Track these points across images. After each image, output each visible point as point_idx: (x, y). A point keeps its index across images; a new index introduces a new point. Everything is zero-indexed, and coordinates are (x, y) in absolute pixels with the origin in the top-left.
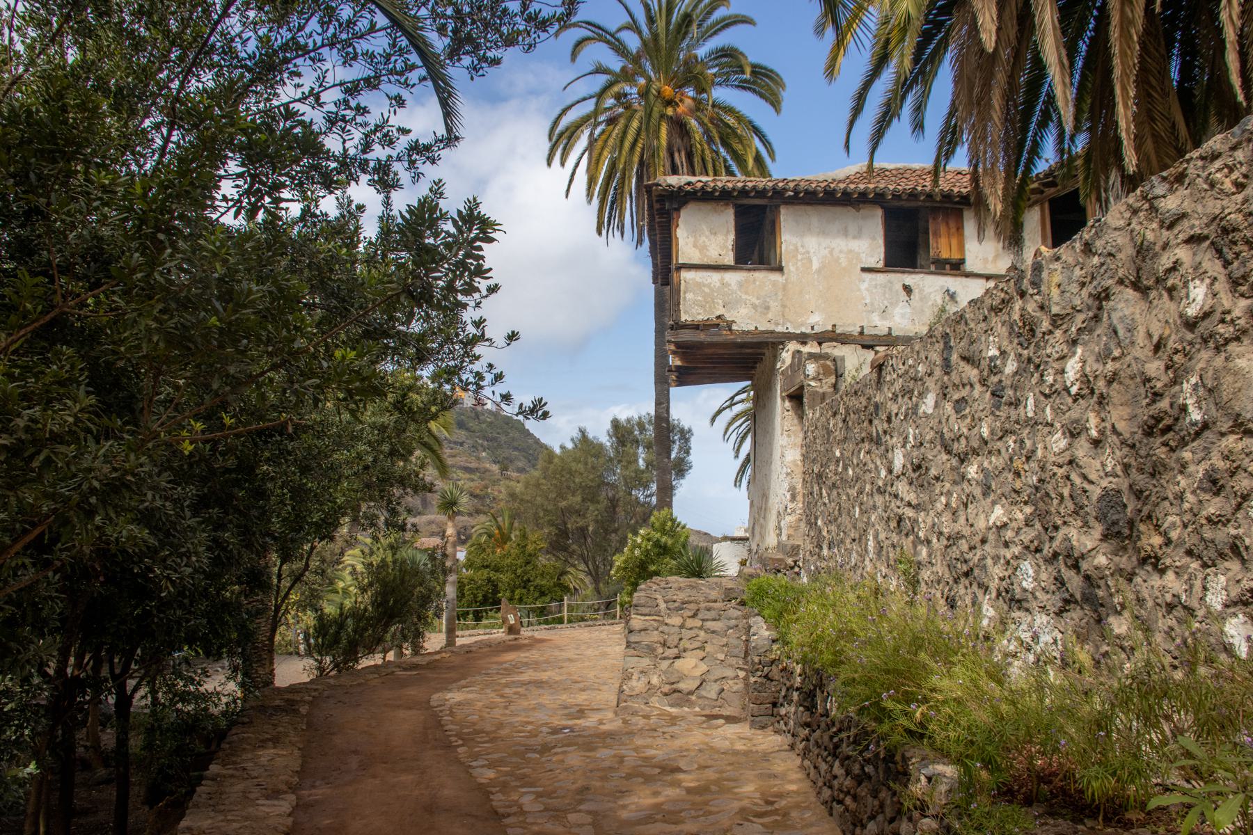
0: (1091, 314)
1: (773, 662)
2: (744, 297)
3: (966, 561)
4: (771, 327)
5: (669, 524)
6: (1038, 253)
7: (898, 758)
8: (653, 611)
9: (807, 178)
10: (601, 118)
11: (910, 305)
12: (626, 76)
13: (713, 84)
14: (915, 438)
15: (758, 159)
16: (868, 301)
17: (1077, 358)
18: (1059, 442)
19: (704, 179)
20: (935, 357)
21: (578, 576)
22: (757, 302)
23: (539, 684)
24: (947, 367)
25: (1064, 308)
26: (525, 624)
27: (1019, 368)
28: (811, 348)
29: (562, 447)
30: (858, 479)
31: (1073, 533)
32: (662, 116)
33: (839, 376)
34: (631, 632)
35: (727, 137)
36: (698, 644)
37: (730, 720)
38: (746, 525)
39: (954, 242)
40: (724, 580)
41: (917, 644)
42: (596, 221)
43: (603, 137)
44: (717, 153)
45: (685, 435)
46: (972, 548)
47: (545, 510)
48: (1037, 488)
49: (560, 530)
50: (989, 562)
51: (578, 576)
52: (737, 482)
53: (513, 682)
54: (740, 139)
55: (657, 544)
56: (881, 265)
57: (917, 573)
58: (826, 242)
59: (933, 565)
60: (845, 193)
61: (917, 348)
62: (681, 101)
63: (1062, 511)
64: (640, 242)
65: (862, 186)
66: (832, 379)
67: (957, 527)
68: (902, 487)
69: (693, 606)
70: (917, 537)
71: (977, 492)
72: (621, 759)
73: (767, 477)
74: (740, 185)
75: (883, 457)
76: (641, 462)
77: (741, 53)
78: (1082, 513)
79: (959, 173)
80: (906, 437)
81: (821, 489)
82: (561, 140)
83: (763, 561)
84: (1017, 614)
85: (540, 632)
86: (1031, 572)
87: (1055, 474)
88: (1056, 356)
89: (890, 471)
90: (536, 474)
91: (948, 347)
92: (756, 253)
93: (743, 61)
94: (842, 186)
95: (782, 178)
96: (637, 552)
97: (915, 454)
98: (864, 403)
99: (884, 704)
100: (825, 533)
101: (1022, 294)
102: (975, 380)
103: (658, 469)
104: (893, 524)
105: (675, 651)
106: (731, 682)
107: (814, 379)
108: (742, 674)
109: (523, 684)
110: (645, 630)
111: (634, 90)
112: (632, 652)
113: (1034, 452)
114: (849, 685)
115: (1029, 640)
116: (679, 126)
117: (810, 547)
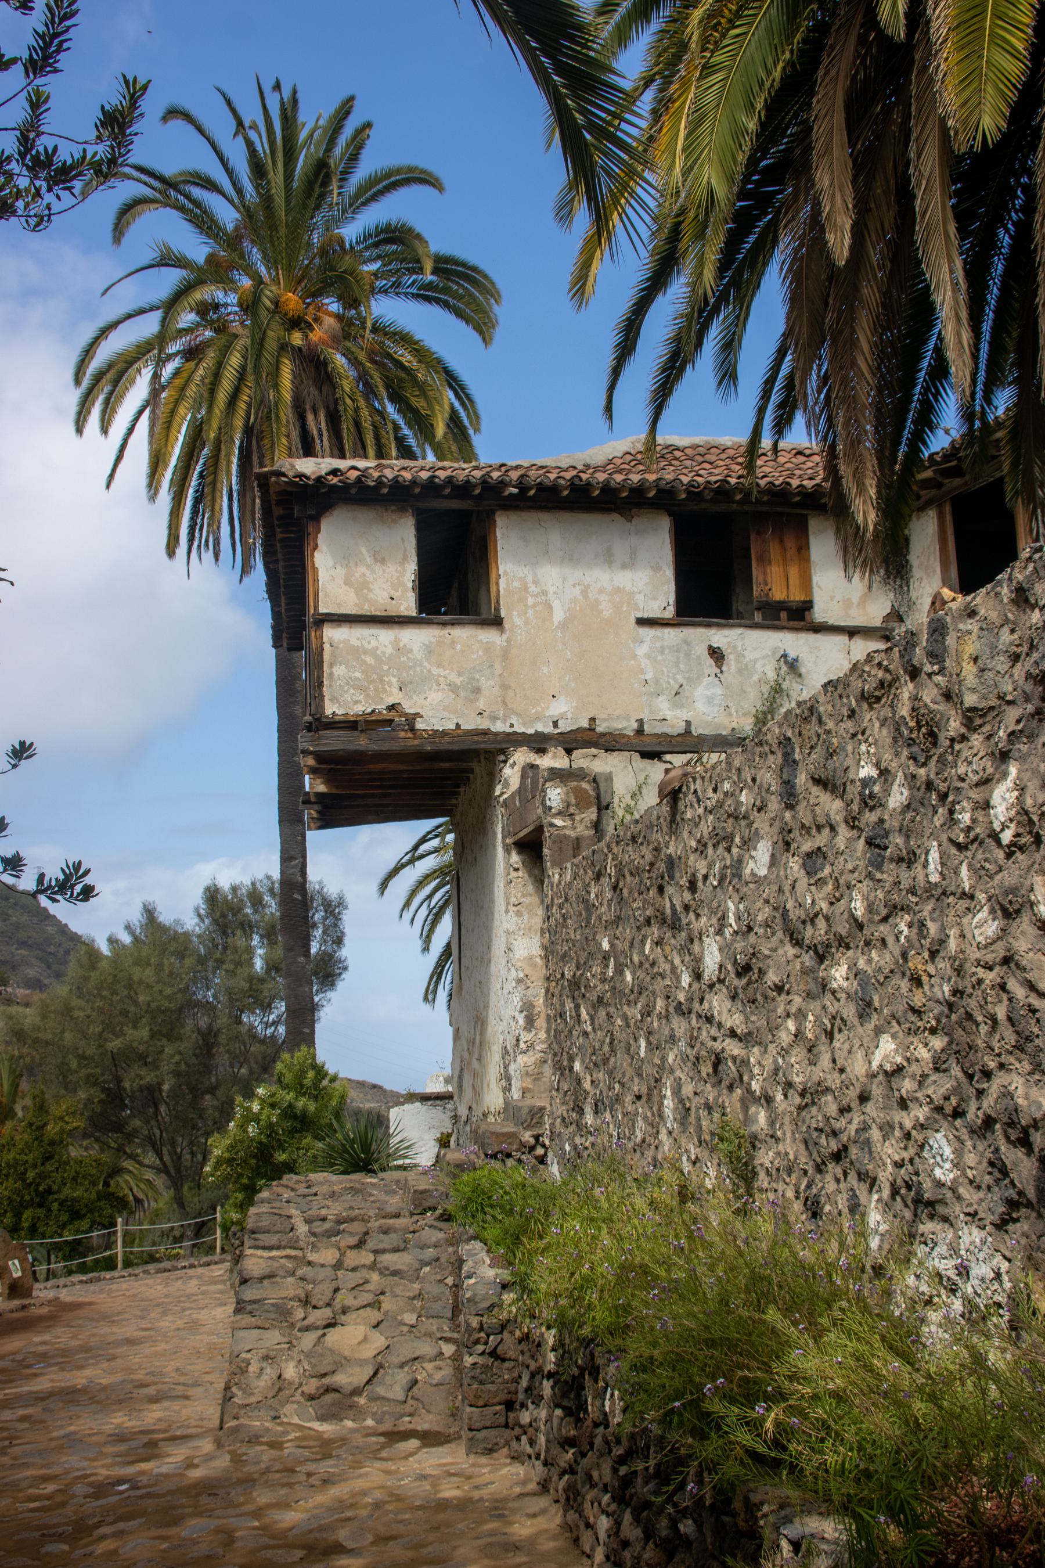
0: (1030, 708)
1: (503, 1327)
2: (435, 671)
3: (835, 1134)
4: (483, 724)
5: (311, 1074)
6: (938, 602)
7: (737, 1505)
8: (285, 1239)
9: (540, 462)
10: (173, 348)
11: (719, 681)
12: (215, 271)
13: (373, 291)
14: (739, 918)
15: (454, 419)
16: (649, 676)
17: (1009, 783)
18: (984, 925)
19: (361, 464)
20: (769, 778)
21: (143, 1177)
22: (458, 680)
23: (70, 1396)
24: (790, 797)
25: (985, 697)
26: (41, 1276)
27: (911, 798)
28: (553, 760)
29: (112, 941)
30: (641, 990)
31: (1017, 1084)
32: (284, 347)
33: (603, 807)
34: (244, 1281)
35: (401, 386)
36: (366, 1298)
37: (430, 1439)
38: (448, 1071)
39: (794, 572)
40: (411, 1175)
41: (760, 1289)
42: (165, 533)
43: (178, 382)
44: (382, 414)
45: (334, 909)
46: (844, 1110)
47: (83, 1057)
48: (951, 1006)
49: (107, 1091)
50: (875, 1134)
51: (143, 1177)
52: (429, 996)
53: (19, 1397)
54: (422, 388)
55: (289, 1113)
56: (670, 613)
57: (752, 1158)
58: (575, 575)
59: (778, 1140)
60: (607, 489)
61: (737, 763)
62: (317, 320)
63: (996, 1046)
64: (246, 569)
65: (635, 478)
66: (592, 814)
67: (817, 1073)
68: (718, 1004)
69: (357, 1227)
70: (749, 1091)
71: (849, 1011)
72: (229, 1539)
73: (482, 987)
74: (424, 475)
75: (686, 949)
76: (258, 964)
77: (418, 237)
78: (1030, 1047)
79: (800, 453)
80: (724, 917)
81: (577, 1007)
82: (99, 386)
83: (478, 1137)
84: (927, 1227)
85: (72, 1290)
86: (948, 1151)
87: (980, 982)
88: (975, 778)
89: (698, 976)
90: (62, 990)
91: (789, 763)
92: (454, 593)
93: (420, 251)
94: (601, 477)
95: (496, 461)
96: (252, 1129)
97: (739, 945)
98: (649, 857)
99: (707, 1406)
100: (587, 1085)
101: (914, 673)
102: (838, 818)
103: (288, 975)
104: (706, 1069)
105: (327, 1312)
106: (429, 1366)
107: (560, 813)
108: (449, 1349)
109: (39, 1398)
110: (271, 1276)
111: (232, 298)
112: (247, 1320)
113: (942, 942)
114: (644, 1370)
115: (952, 1273)
116: (314, 367)
117: (562, 1110)
